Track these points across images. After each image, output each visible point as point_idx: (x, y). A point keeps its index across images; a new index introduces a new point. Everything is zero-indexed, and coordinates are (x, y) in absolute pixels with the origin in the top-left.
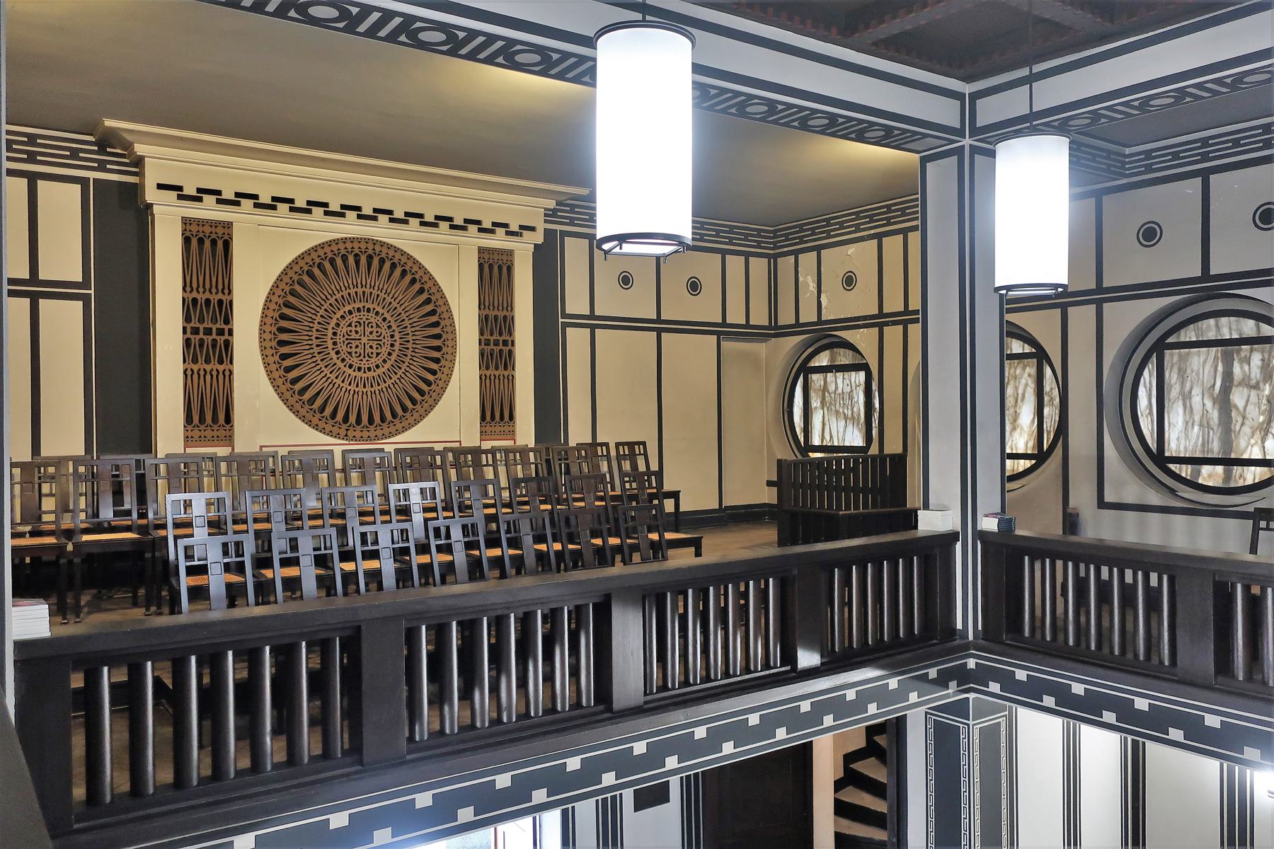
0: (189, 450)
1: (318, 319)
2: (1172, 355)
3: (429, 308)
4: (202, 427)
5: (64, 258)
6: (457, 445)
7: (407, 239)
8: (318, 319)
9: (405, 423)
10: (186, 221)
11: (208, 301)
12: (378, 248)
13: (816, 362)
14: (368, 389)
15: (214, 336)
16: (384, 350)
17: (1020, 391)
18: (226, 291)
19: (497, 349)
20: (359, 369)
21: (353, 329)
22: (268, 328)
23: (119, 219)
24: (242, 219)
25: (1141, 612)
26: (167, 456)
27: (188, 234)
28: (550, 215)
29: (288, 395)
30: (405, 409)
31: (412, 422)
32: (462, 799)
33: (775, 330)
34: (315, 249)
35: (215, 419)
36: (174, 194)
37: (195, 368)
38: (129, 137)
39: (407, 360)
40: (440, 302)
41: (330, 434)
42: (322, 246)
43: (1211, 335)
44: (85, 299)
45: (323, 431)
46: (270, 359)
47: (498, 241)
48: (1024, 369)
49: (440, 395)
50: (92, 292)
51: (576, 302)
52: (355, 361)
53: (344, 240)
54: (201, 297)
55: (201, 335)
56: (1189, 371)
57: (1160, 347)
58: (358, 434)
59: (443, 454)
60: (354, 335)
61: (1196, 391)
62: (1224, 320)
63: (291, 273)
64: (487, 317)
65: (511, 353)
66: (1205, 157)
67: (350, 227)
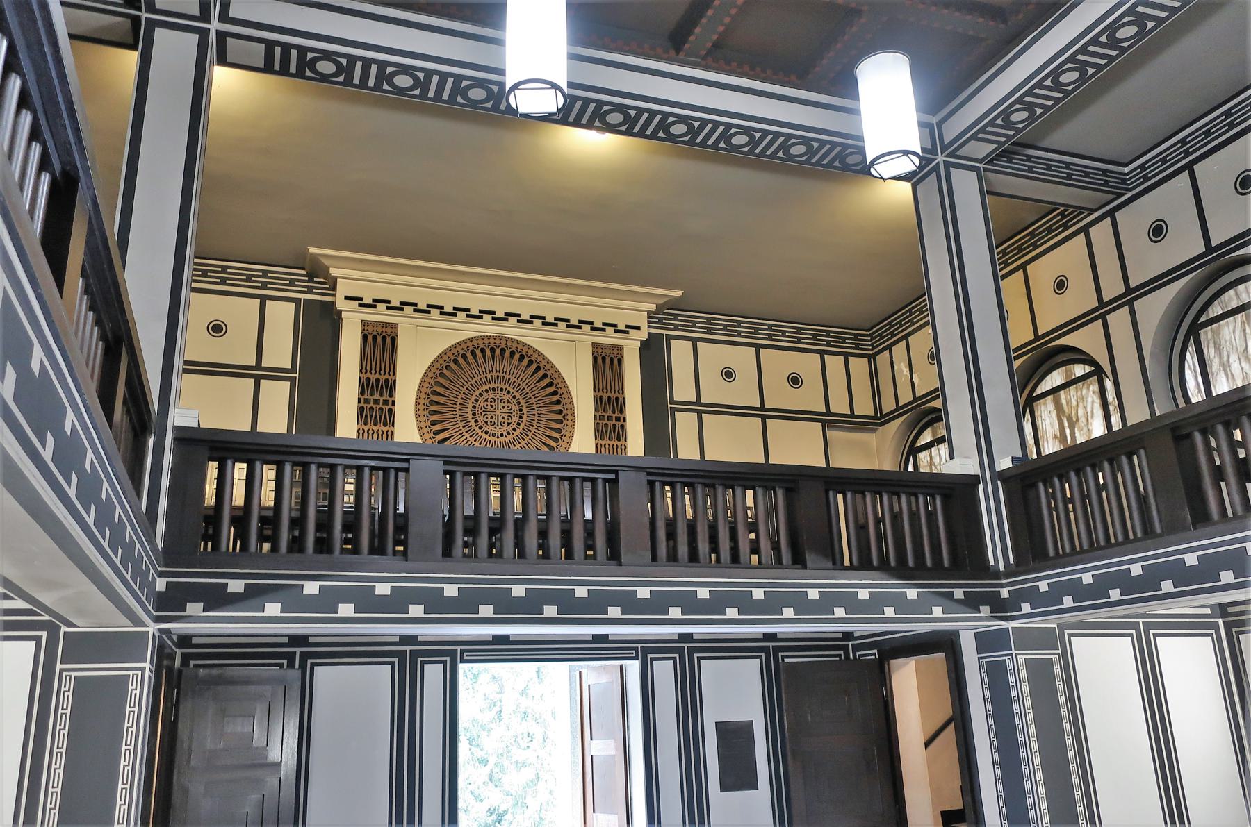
1: (461, 395)
2: (1206, 333)
5: (280, 353)
7: (533, 337)
8: (461, 395)
12: (509, 344)
13: (921, 442)
16: (514, 421)
17: (1089, 410)
19: (376, 407)
22: (422, 401)
23: (320, 326)
24: (406, 323)
25: (1155, 513)
32: (486, 597)
33: (879, 420)
34: (460, 344)
37: (366, 428)
38: (326, 262)
39: (533, 429)
42: (465, 341)
43: (1234, 304)
44: (292, 380)
46: (423, 425)
47: (609, 338)
48: (1089, 386)
51: (683, 390)
53: (483, 338)
54: (373, 377)
56: (1223, 342)
57: (1195, 330)
61: (1233, 358)
62: (1241, 287)
65: (623, 427)
66: (1187, 154)
67: (486, 328)
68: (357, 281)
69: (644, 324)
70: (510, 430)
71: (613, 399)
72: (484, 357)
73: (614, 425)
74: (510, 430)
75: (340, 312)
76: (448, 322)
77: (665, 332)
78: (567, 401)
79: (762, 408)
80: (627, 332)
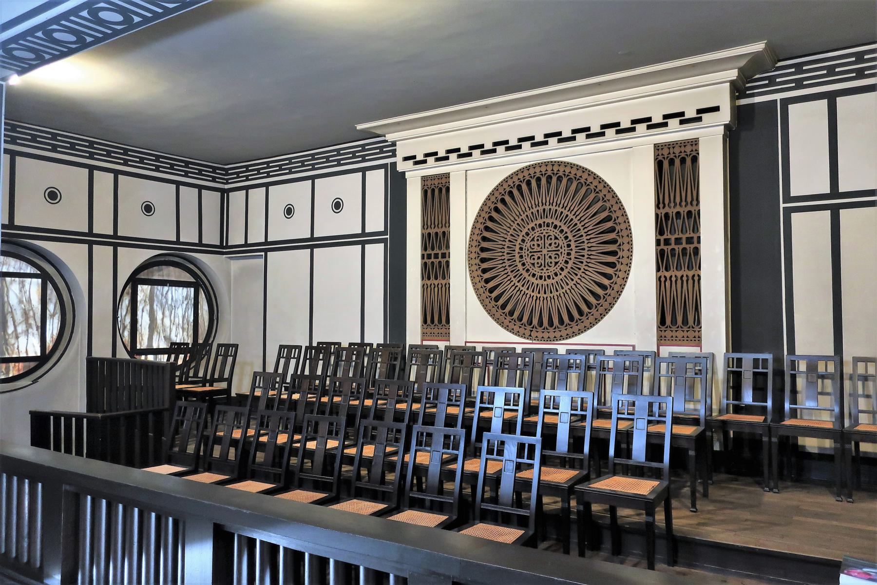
0: (425, 343)
6: (631, 349)
7: (579, 154)
9: (581, 326)
10: (657, 147)
12: (556, 168)
14: (548, 294)
15: (684, 245)
16: (562, 259)
18: (695, 203)
19: (436, 261)
20: (541, 277)
23: (396, 185)
24: (454, 168)
26: (319, 343)
27: (660, 158)
28: (738, 90)
30: (581, 313)
31: (588, 325)
35: (440, 321)
36: (411, 162)
37: (668, 274)
41: (517, 334)
45: (512, 331)
47: (675, 133)
50: (782, 205)
51: (807, 174)
52: (536, 270)
53: (528, 168)
55: (684, 245)
58: (540, 335)
59: (485, 352)
60: (536, 248)
63: (605, 191)
64: (429, 234)
67: (528, 157)
70: (558, 270)
72: (530, 190)
73: (684, 249)
74: (558, 270)
75: (404, 173)
77: (778, 97)
80: (699, 119)
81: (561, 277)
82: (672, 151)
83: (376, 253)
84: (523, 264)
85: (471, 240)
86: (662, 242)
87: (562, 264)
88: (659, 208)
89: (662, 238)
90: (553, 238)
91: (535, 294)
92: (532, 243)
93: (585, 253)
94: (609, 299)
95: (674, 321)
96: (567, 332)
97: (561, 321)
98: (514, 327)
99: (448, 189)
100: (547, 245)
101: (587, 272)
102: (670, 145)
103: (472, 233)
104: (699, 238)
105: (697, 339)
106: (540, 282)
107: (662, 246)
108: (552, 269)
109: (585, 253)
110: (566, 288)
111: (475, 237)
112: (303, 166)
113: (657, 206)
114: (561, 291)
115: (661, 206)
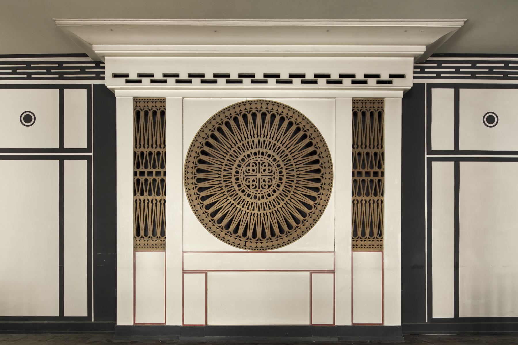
3: (311, 149)
4: (146, 238)
5: (77, 137)
9: (290, 237)
10: (355, 101)
11: (150, 154)
12: (270, 107)
16: (274, 183)
18: (380, 146)
19: (150, 179)
21: (251, 168)
23: (103, 105)
24: (170, 92)
28: (420, 64)
29: (314, 216)
30: (290, 227)
36: (123, 79)
37: (142, 198)
38: (85, 37)
40: (320, 145)
45: (228, 242)
47: (370, 91)
49: (319, 216)
51: (441, 138)
52: (252, 191)
53: (245, 103)
54: (146, 151)
55: (154, 177)
58: (254, 245)
60: (251, 173)
67: (247, 93)
68: (132, 57)
69: (410, 72)
70: (271, 192)
71: (154, 154)
73: (372, 181)
74: (271, 192)
76: (209, 90)
78: (325, 160)
79: (457, 151)
81: (273, 197)
82: (364, 105)
83: (77, 171)
84: (239, 186)
85: (188, 161)
86: (138, 174)
87: (274, 187)
88: (136, 148)
89: (138, 171)
90: (267, 165)
91: (250, 211)
92: (248, 168)
93: (294, 179)
94: (314, 216)
95: (363, 234)
96: (277, 242)
97: (273, 234)
98: (230, 239)
99: (163, 113)
100: (261, 171)
101: (296, 195)
102: (146, 100)
103: (189, 156)
104: (165, 173)
105: (163, 246)
106: (255, 201)
107: (138, 177)
108: (265, 191)
109: (294, 179)
110: (278, 206)
111: (192, 159)
112: (14, 72)
113: (135, 146)
114: (273, 209)
115: (138, 146)
